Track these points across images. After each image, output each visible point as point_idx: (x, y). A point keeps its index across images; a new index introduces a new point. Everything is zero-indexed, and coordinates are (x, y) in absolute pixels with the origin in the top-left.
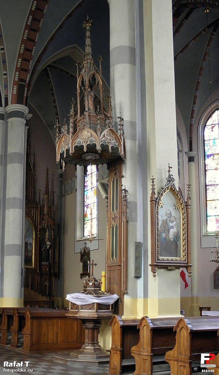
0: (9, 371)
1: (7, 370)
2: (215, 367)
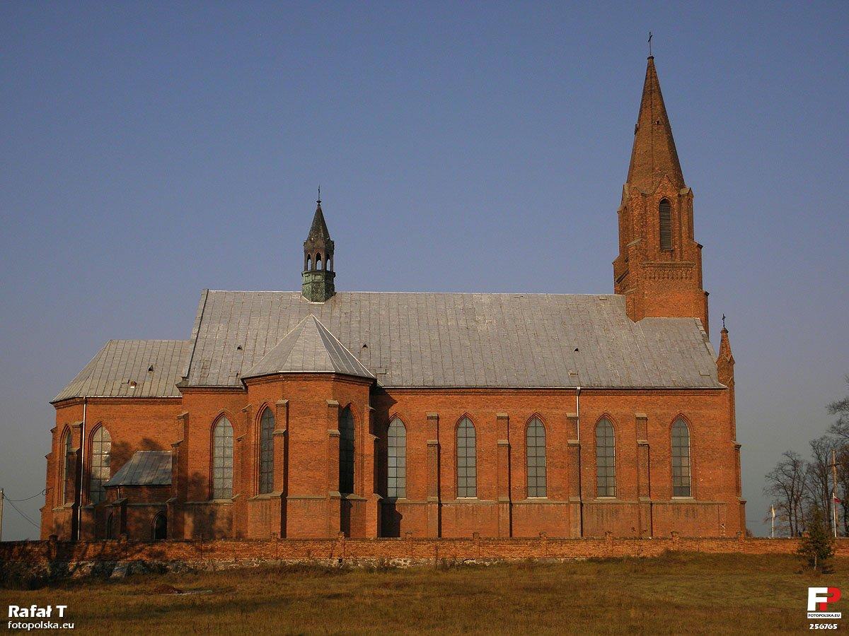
0: (21, 626)
1: (15, 626)
2: (840, 617)
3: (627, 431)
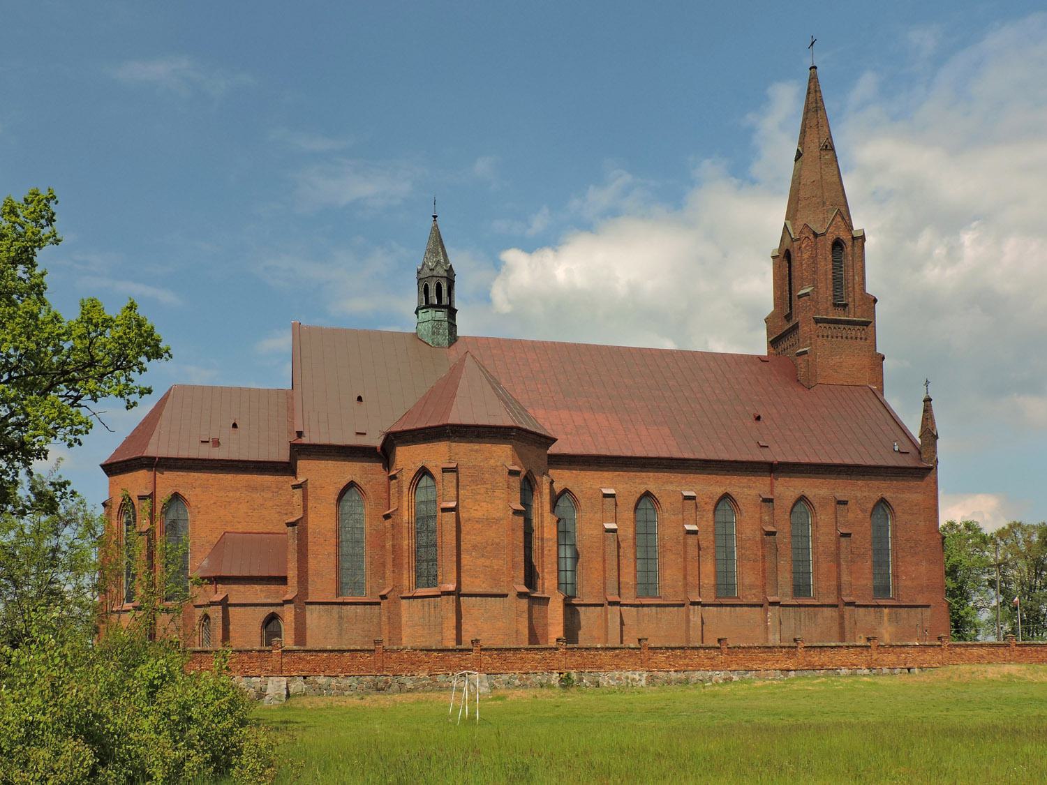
3: (824, 517)
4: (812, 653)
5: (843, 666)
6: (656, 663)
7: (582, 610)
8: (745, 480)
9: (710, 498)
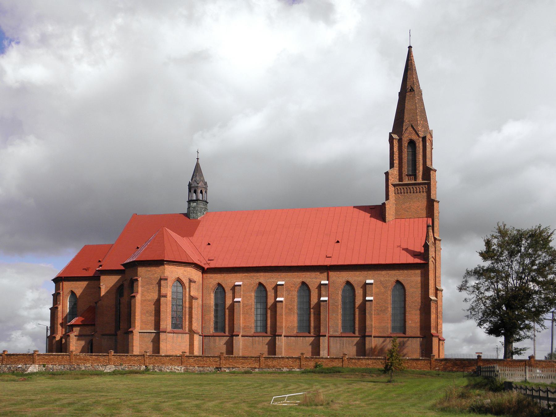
4: (268, 360)
5: (285, 367)
6: (189, 363)
7: (419, 335)
8: (314, 275)
9: (294, 284)
